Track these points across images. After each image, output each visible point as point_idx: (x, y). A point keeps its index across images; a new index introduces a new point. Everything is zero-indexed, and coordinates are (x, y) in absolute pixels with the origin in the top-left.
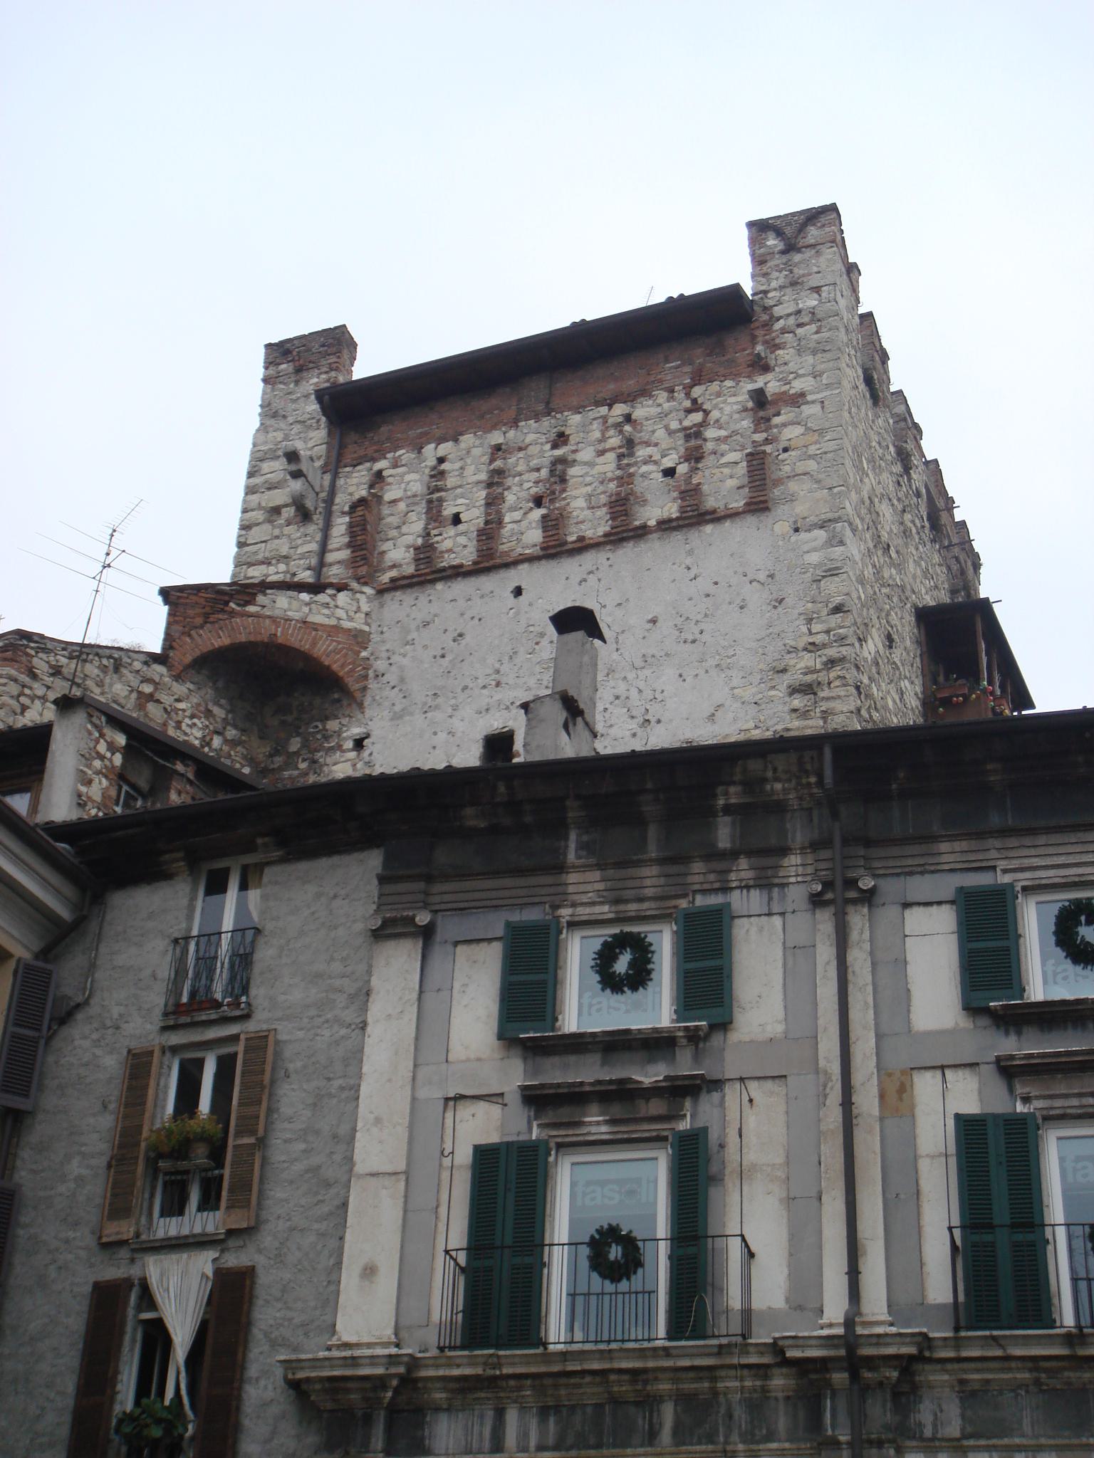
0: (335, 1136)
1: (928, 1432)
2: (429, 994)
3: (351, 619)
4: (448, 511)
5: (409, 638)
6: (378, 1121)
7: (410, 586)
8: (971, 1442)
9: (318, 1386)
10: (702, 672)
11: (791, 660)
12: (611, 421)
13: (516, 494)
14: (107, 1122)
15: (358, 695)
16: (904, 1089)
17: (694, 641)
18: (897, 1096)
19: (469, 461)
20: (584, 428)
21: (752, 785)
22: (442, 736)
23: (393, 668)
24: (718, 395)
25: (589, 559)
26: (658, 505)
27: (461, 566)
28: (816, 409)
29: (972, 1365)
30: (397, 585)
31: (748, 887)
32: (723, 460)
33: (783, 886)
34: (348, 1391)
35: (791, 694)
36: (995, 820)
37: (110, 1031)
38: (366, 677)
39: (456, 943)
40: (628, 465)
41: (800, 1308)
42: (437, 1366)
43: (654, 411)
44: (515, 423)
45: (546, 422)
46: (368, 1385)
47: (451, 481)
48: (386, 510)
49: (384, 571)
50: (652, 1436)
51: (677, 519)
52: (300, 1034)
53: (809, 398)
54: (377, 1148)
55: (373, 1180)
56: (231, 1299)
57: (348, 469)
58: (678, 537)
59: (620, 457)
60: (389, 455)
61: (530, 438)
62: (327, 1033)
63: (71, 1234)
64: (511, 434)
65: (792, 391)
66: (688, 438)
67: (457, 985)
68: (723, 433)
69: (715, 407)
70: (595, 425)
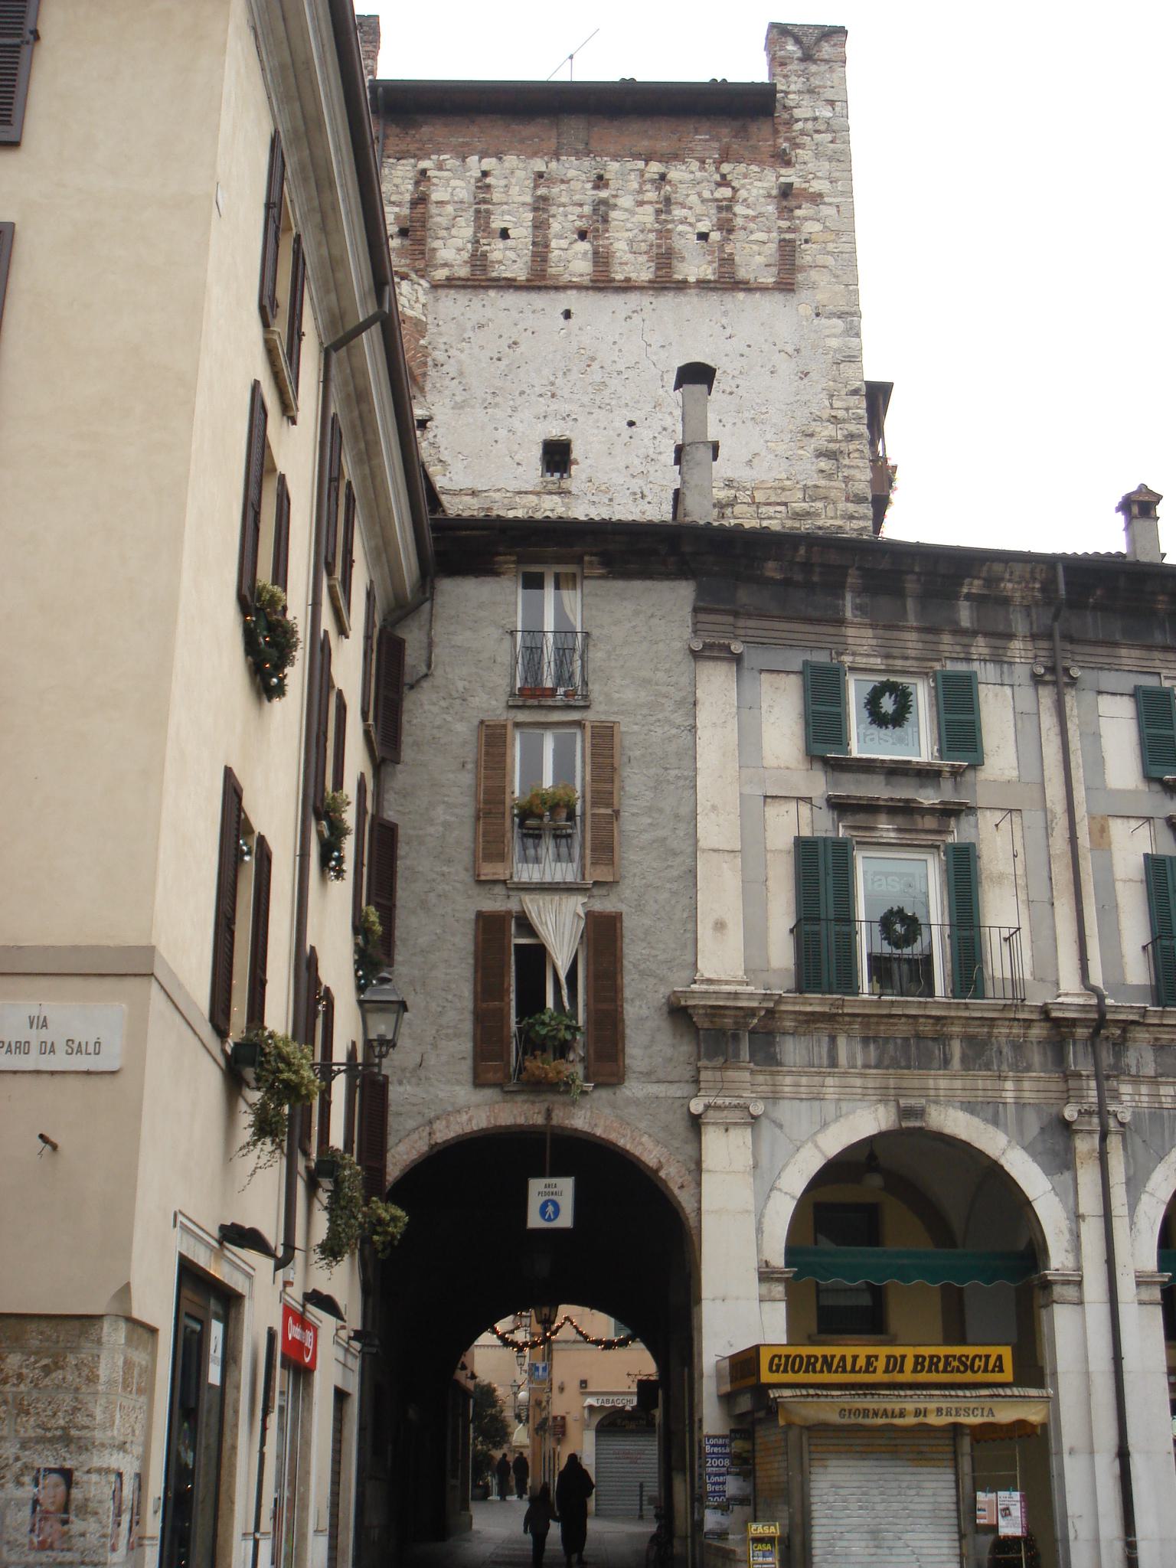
0: (677, 816)
1: (1133, 1071)
2: (747, 708)
3: (412, 308)
4: (497, 224)
5: (466, 336)
6: (714, 808)
7: (464, 287)
8: (1163, 1079)
9: (701, 1011)
10: (739, 423)
11: (816, 427)
12: (647, 176)
13: (562, 223)
14: (467, 778)
15: (420, 379)
16: (1103, 830)
17: (731, 393)
18: (1101, 833)
19: (513, 181)
20: (623, 175)
21: (991, 581)
22: (502, 433)
23: (452, 361)
24: (745, 176)
25: (633, 299)
26: (695, 266)
27: (515, 280)
28: (832, 211)
29: (1166, 1029)
30: (451, 283)
31: (985, 661)
32: (753, 237)
33: (1011, 663)
34: (725, 1016)
35: (817, 457)
36: (1158, 638)
37: (458, 701)
38: (425, 364)
39: (761, 671)
40: (666, 221)
41: (1042, 980)
42: (795, 1003)
43: (688, 177)
44: (556, 155)
45: (587, 163)
46: (741, 1013)
47: (497, 196)
48: (433, 210)
49: (436, 267)
50: (946, 1062)
51: (715, 281)
52: (636, 728)
53: (826, 200)
54: (716, 829)
55: (715, 855)
56: (603, 936)
57: (391, 160)
58: (714, 297)
59: (658, 212)
60: (434, 157)
61: (572, 173)
62: (660, 731)
63: (445, 869)
64: (553, 165)
65: (811, 190)
66: (720, 209)
67: (764, 706)
68: (751, 212)
69: (743, 186)
70: (633, 176)
